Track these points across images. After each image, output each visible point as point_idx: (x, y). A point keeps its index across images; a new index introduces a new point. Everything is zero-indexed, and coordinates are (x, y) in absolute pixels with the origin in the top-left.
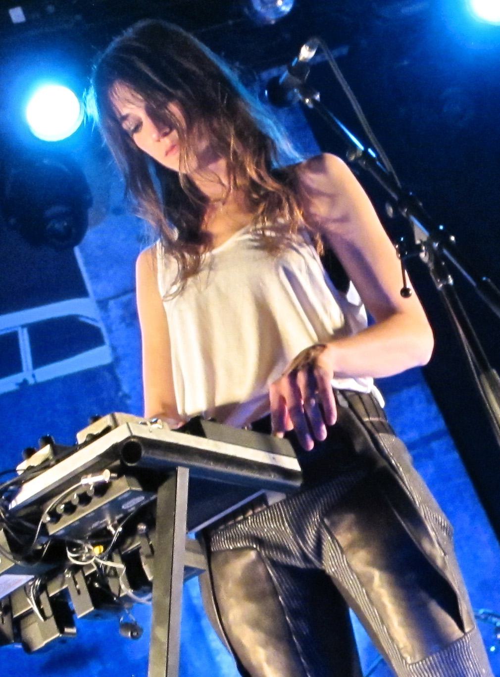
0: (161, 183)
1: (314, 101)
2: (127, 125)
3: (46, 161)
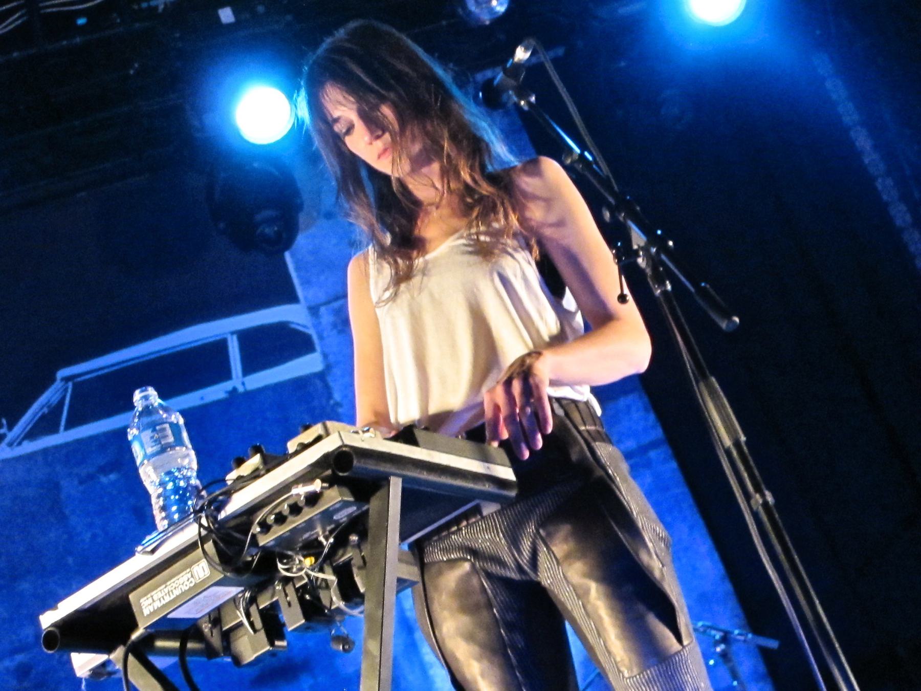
1: (529, 103)
2: (339, 128)
3: (256, 165)
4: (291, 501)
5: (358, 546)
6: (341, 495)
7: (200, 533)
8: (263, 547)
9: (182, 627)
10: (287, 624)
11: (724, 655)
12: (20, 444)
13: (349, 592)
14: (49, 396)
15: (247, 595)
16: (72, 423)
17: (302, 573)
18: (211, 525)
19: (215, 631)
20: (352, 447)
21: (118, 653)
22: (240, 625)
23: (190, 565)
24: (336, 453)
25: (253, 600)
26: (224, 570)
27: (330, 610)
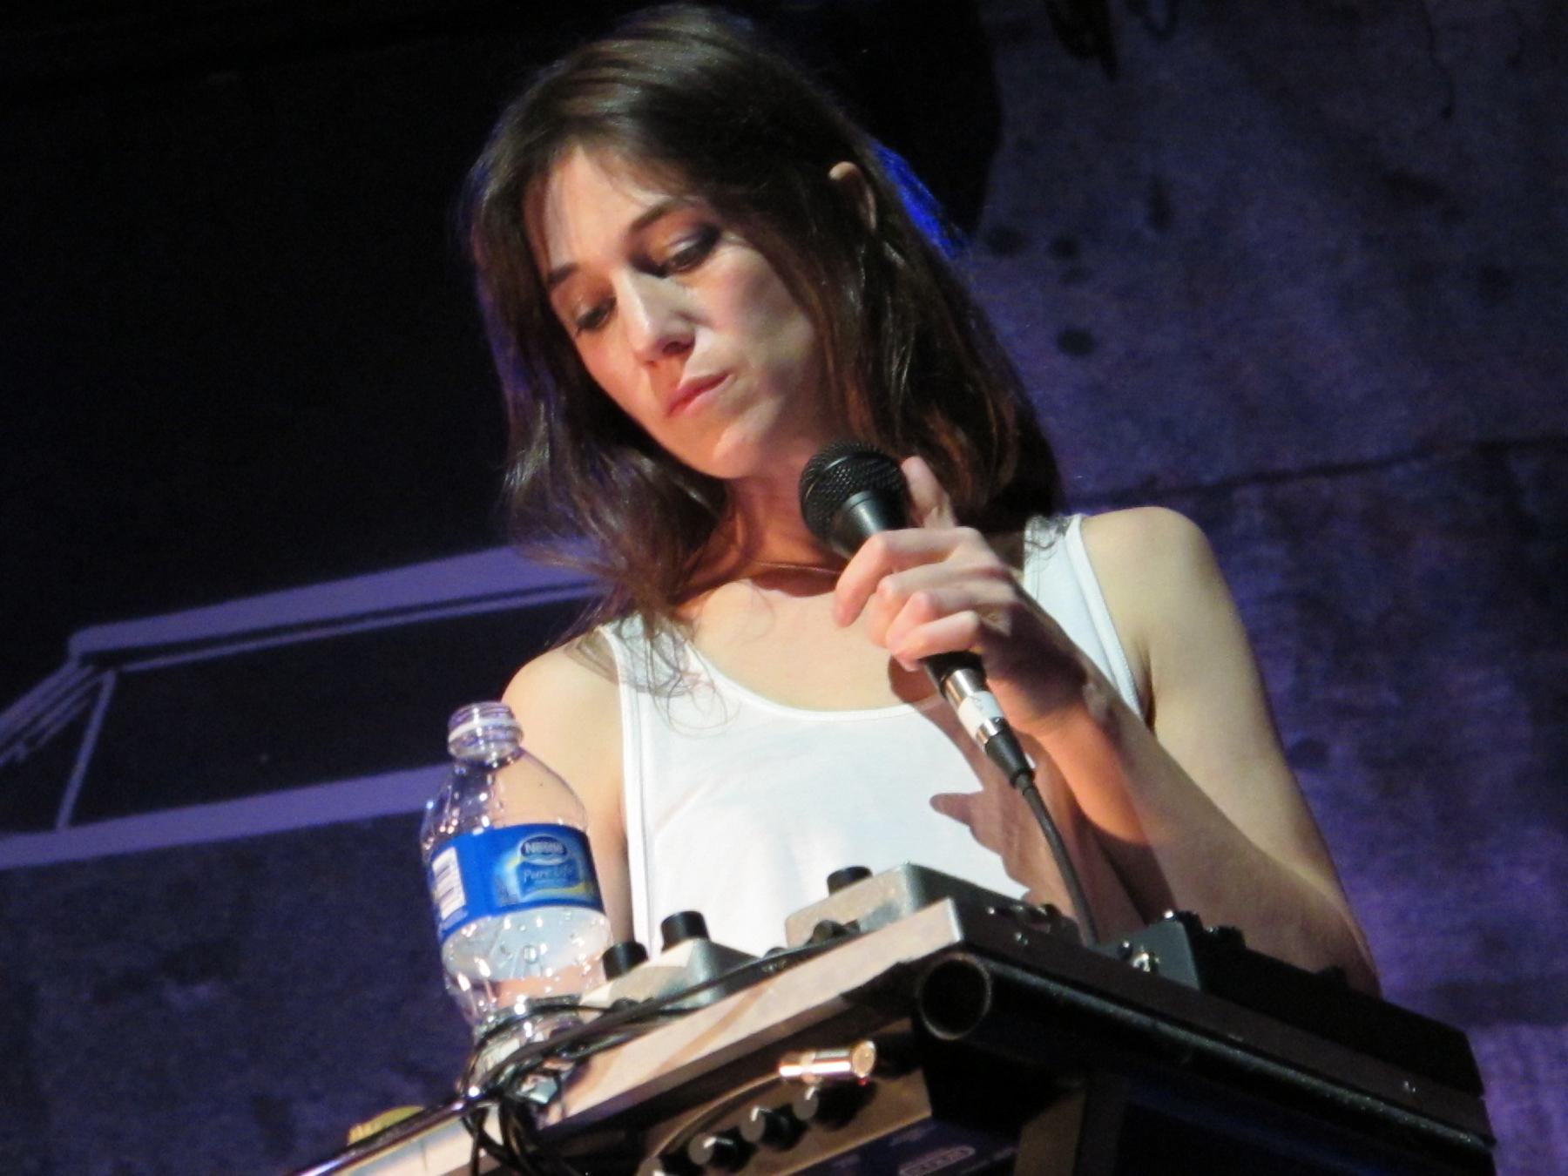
0: (1332, 865)
7: (475, 1160)
18: (514, 1144)
24: (934, 964)
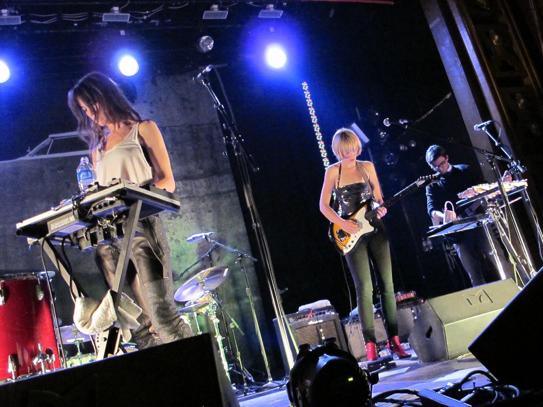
4: (105, 202)
5: (125, 219)
6: (121, 203)
7: (73, 207)
8: (93, 215)
9: (64, 235)
10: (98, 240)
11: (240, 261)
12: (33, 156)
13: (120, 233)
14: (45, 142)
15: (87, 228)
16: (51, 152)
17: (106, 225)
19: (75, 238)
20: (128, 189)
21: (41, 240)
22: (83, 237)
23: (69, 216)
25: (88, 230)
26: (80, 220)
27: (113, 238)
